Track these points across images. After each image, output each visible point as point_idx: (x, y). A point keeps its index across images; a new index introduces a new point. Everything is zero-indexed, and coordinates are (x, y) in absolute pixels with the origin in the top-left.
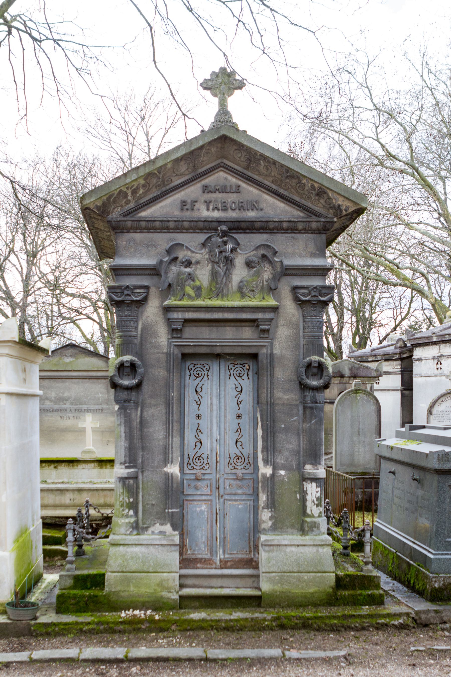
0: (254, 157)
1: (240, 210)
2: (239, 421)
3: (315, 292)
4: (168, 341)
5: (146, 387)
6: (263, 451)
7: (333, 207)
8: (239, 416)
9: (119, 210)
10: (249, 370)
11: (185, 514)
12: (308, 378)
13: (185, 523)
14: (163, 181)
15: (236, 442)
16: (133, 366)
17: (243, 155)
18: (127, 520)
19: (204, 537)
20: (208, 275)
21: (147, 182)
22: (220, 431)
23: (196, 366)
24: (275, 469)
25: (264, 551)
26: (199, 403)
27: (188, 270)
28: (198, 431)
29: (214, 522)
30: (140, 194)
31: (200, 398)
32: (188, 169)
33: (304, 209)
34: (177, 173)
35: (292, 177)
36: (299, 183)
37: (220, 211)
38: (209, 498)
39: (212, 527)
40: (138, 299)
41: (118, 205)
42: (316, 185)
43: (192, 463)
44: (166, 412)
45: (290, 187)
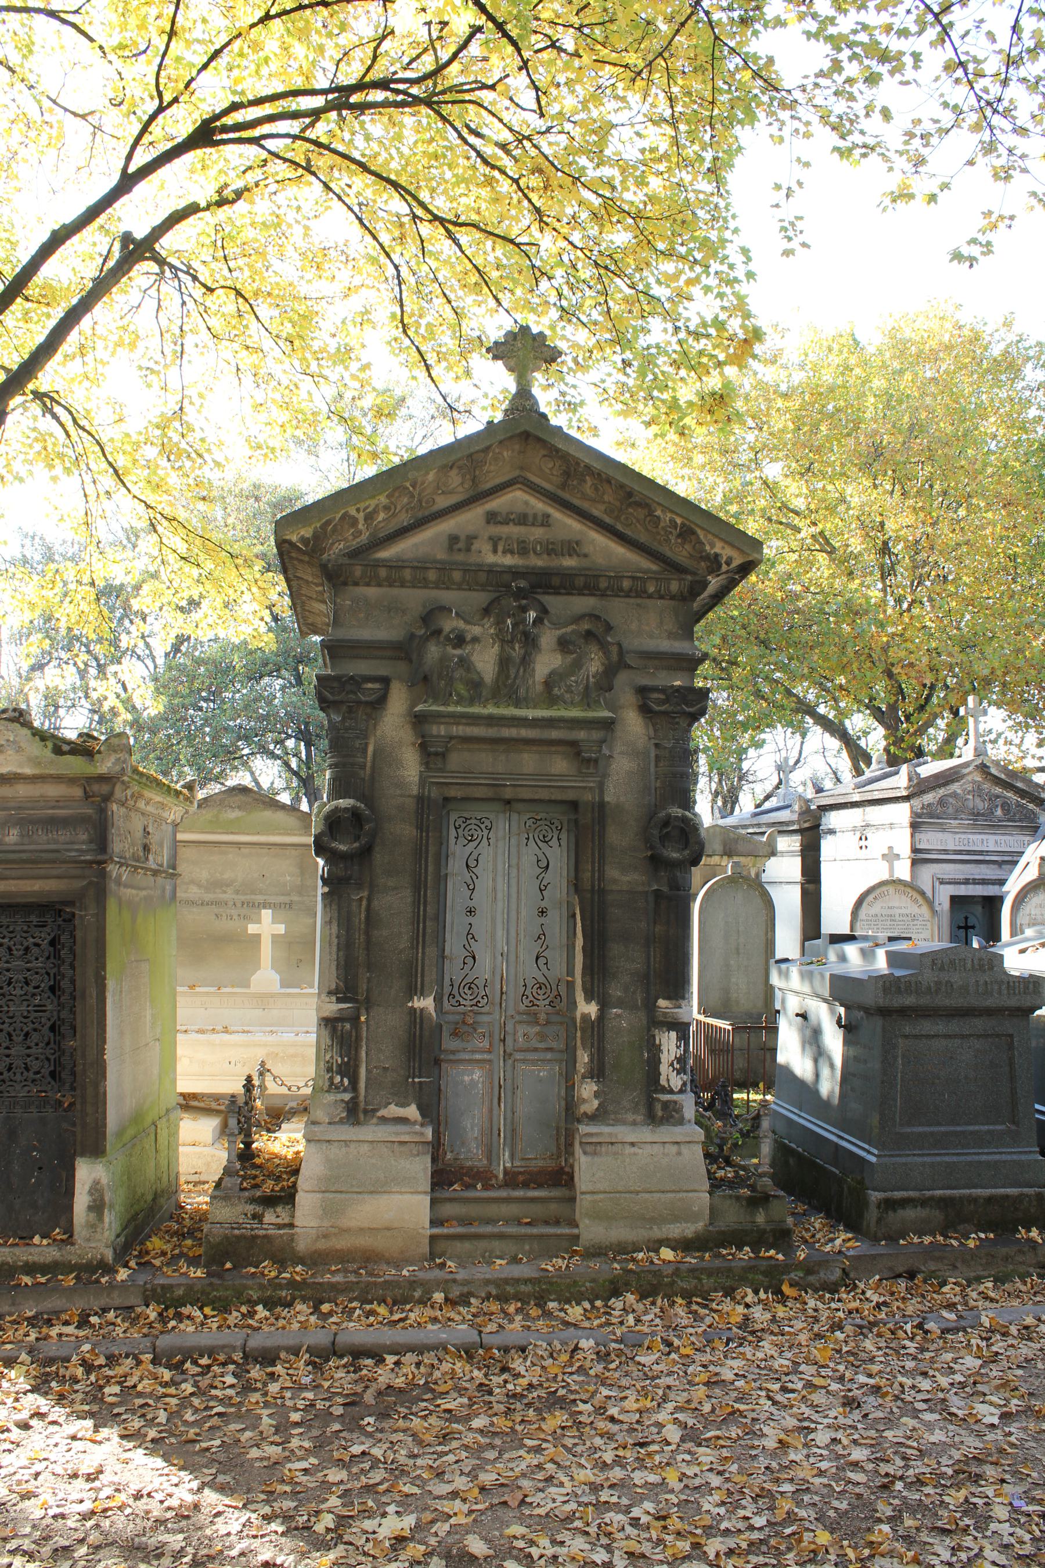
2: (542, 920)
6: (584, 975)
7: (707, 558)
14: (420, 501)
16: (355, 815)
18: (340, 1096)
24: (604, 1006)
27: (458, 652)
35: (638, 504)
38: (486, 1056)
39: (491, 1111)
42: (679, 521)
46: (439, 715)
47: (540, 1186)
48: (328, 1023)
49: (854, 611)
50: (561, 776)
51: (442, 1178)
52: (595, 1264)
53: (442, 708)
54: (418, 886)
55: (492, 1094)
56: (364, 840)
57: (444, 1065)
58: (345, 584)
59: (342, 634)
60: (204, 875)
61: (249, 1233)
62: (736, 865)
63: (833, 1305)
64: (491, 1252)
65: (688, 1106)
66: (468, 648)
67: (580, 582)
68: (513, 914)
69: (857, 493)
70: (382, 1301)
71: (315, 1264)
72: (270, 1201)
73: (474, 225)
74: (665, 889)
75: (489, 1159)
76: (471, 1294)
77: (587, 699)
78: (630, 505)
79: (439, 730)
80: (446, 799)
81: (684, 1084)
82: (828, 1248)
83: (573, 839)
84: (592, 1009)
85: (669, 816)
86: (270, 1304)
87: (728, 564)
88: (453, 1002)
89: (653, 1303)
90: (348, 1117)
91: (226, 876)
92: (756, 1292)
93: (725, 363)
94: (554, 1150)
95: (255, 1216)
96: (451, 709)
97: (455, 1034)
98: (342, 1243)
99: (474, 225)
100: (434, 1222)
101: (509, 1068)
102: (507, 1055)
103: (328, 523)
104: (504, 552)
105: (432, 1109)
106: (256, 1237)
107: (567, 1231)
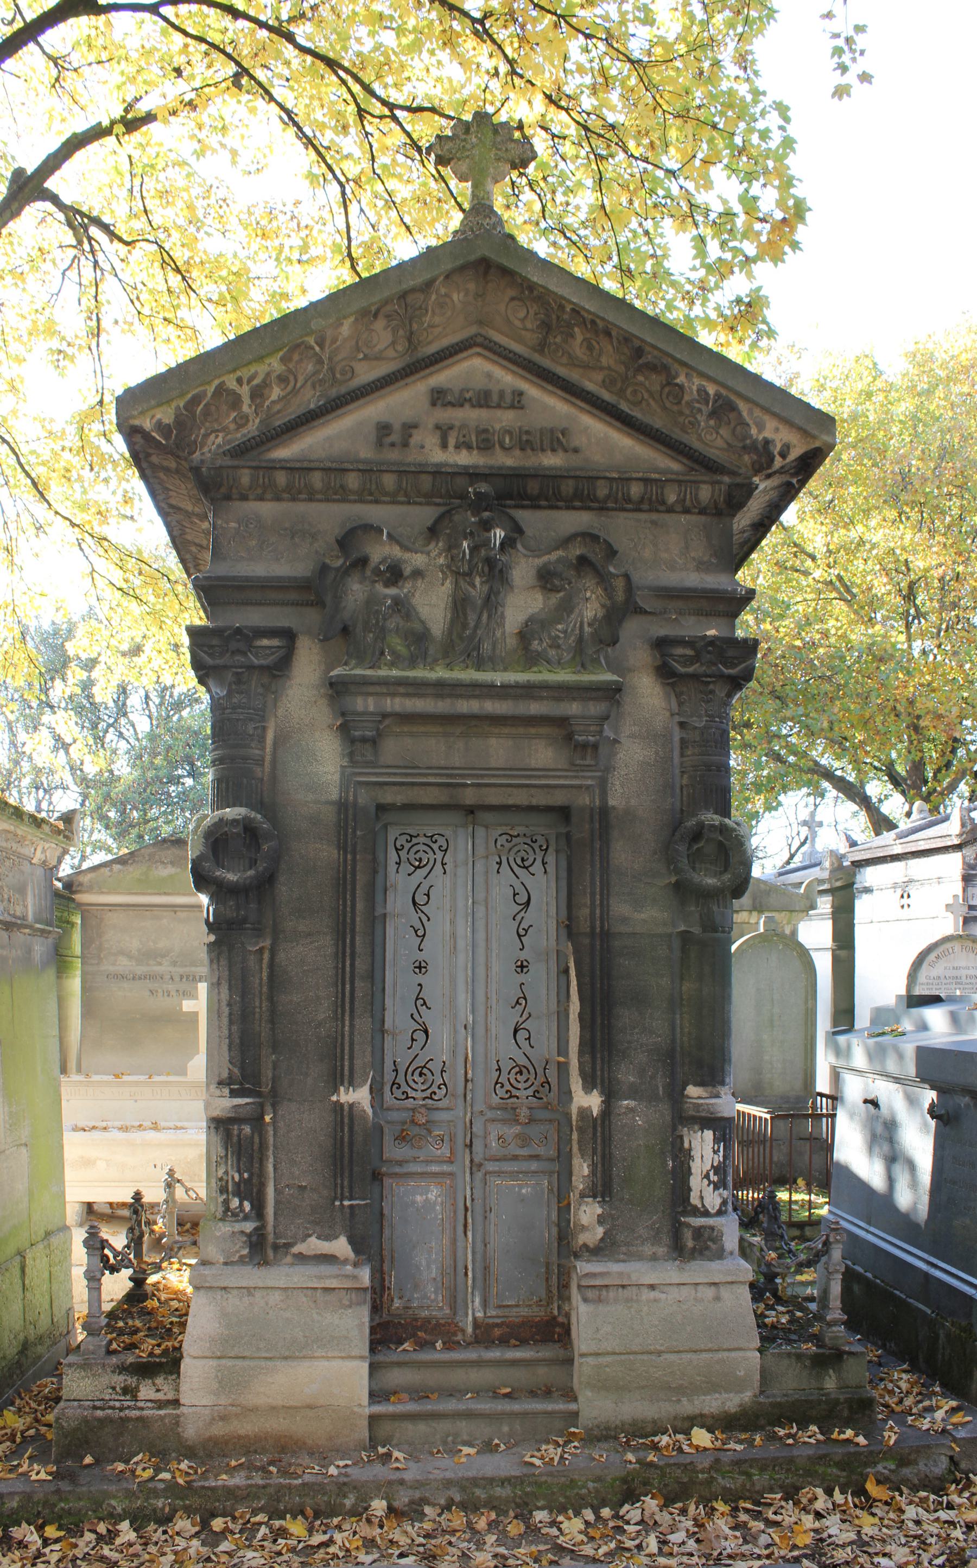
0: (558, 318)
1: (522, 449)
2: (522, 978)
3: (709, 652)
4: (342, 774)
5: (284, 889)
6: (581, 1053)
7: (752, 448)
8: (522, 967)
9: (220, 440)
10: (546, 850)
11: (386, 1211)
12: (694, 869)
13: (387, 1232)
14: (332, 370)
15: (516, 1031)
16: (249, 830)
17: (532, 312)
18: (238, 1227)
19: (433, 1266)
20: (443, 606)
21: (290, 371)
22: (473, 1005)
23: (415, 841)
24: (610, 1097)
25: (585, 1300)
26: (420, 933)
27: (392, 591)
28: (420, 1002)
29: (460, 1228)
30: (273, 402)
31: (424, 919)
32: (393, 343)
33: (681, 453)
34: (366, 351)
35: (653, 368)
36: (669, 384)
37: (475, 452)
38: (446, 1168)
39: (454, 1241)
40: (263, 662)
41: (216, 426)
42: (711, 390)
43: (403, 1084)
44: (337, 954)
45: (646, 396)
46: (365, 682)
47: (523, 1342)
48: (221, 1125)
49: (880, 655)
50: (546, 771)
51: (386, 1333)
52: (601, 1453)
53: (369, 672)
54: (342, 931)
55: (456, 1218)
56: (262, 866)
57: (387, 1181)
58: (228, 498)
59: (223, 569)
60: (134, 944)
61: (116, 1414)
62: (769, 920)
63: (943, 1515)
64: (456, 1435)
65: (730, 1230)
66: (407, 586)
67: (568, 488)
68: (481, 970)
69: (880, 532)
70: (299, 1512)
71: (210, 1456)
72: (146, 1370)
73: (433, 110)
74: (696, 930)
75: (453, 1307)
76: (424, 1501)
77: (581, 655)
78: (639, 370)
79: (365, 704)
80: (382, 808)
81: (724, 1203)
82: (925, 1424)
83: (563, 864)
84: (593, 1101)
85: (701, 825)
86: (139, 1521)
87: (783, 455)
88: (398, 1094)
89: (684, 1512)
90: (251, 1255)
91: (161, 945)
92: (829, 1492)
93: (754, 260)
94: (543, 1293)
95: (125, 1390)
96: (383, 672)
97: (402, 1138)
98: (246, 1428)
99: (433, 110)
100: (374, 1396)
101: (478, 1183)
102: (475, 1166)
103: (196, 400)
104: (457, 447)
105: (370, 1242)
106: (128, 1419)
107: (561, 1406)
